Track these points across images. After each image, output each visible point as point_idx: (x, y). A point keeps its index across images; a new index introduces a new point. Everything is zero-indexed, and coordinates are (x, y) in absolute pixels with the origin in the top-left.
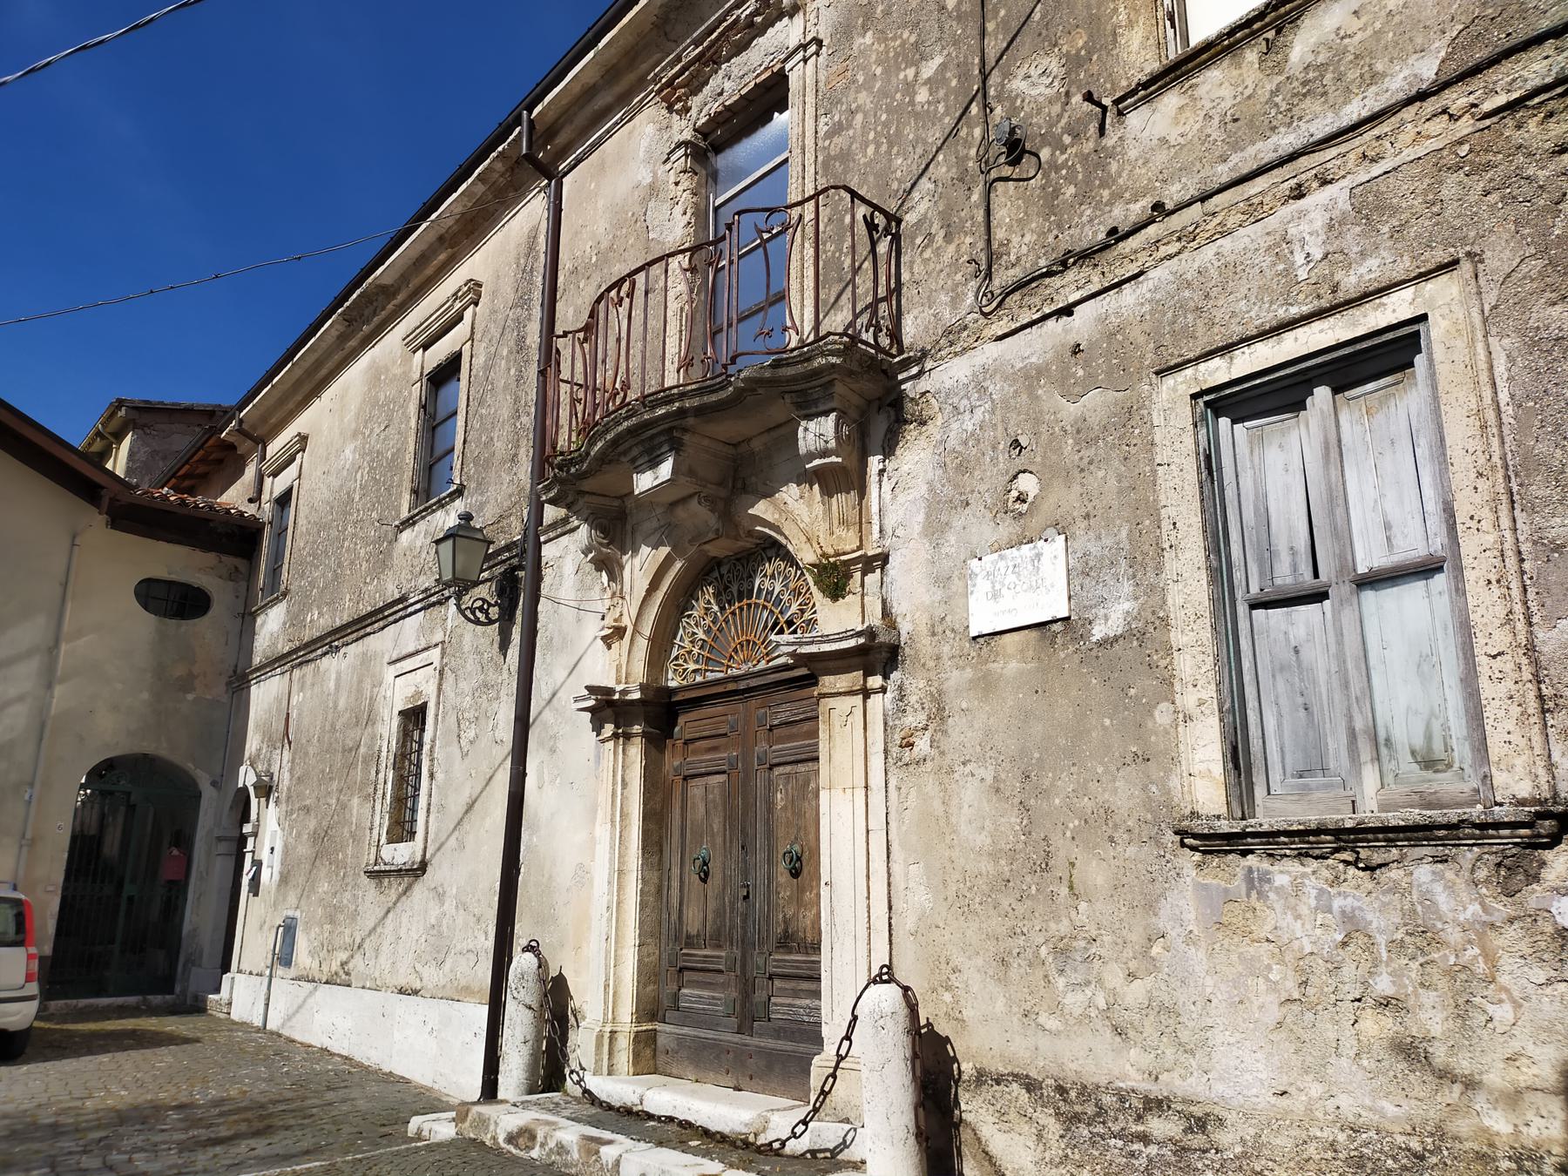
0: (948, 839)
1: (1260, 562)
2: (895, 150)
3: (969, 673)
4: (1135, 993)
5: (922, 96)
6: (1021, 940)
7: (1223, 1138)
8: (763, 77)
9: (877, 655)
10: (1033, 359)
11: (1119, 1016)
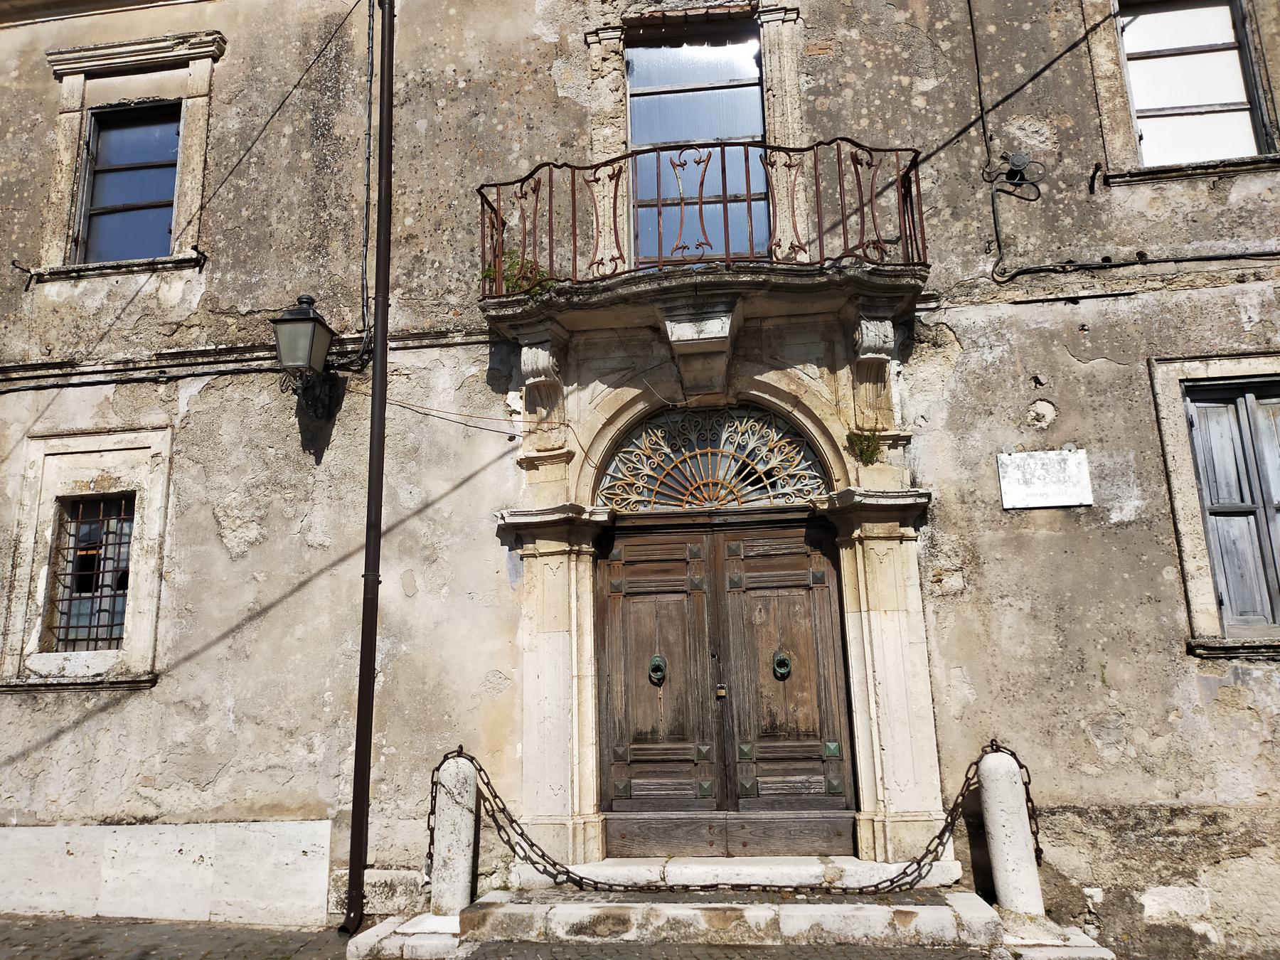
0: (990, 650)
2: (892, 132)
3: (1002, 534)
4: (1158, 745)
5: (919, 102)
6: (1064, 718)
7: (1230, 825)
8: (718, 11)
9: (915, 514)
10: (1047, 325)
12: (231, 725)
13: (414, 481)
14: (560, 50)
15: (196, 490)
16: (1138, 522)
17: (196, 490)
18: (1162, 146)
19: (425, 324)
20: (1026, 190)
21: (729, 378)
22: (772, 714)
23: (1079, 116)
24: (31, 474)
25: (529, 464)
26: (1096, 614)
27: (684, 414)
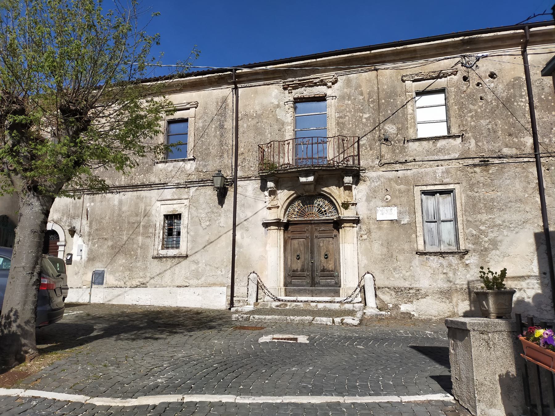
1: (159, 87)
3: (376, 226)
4: (408, 274)
5: (364, 120)
7: (421, 291)
9: (357, 221)
11: (405, 277)
12: (204, 266)
13: (243, 212)
14: (278, 106)
15: (195, 214)
16: (408, 224)
17: (195, 214)
18: (423, 132)
19: (246, 175)
20: (388, 143)
21: (315, 189)
22: (324, 267)
23: (403, 124)
24: (158, 209)
25: (270, 208)
26: (396, 245)
27: (306, 196)
